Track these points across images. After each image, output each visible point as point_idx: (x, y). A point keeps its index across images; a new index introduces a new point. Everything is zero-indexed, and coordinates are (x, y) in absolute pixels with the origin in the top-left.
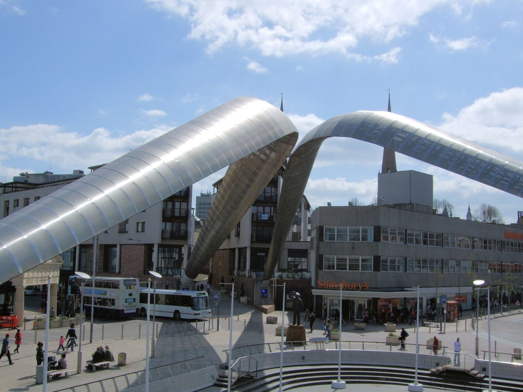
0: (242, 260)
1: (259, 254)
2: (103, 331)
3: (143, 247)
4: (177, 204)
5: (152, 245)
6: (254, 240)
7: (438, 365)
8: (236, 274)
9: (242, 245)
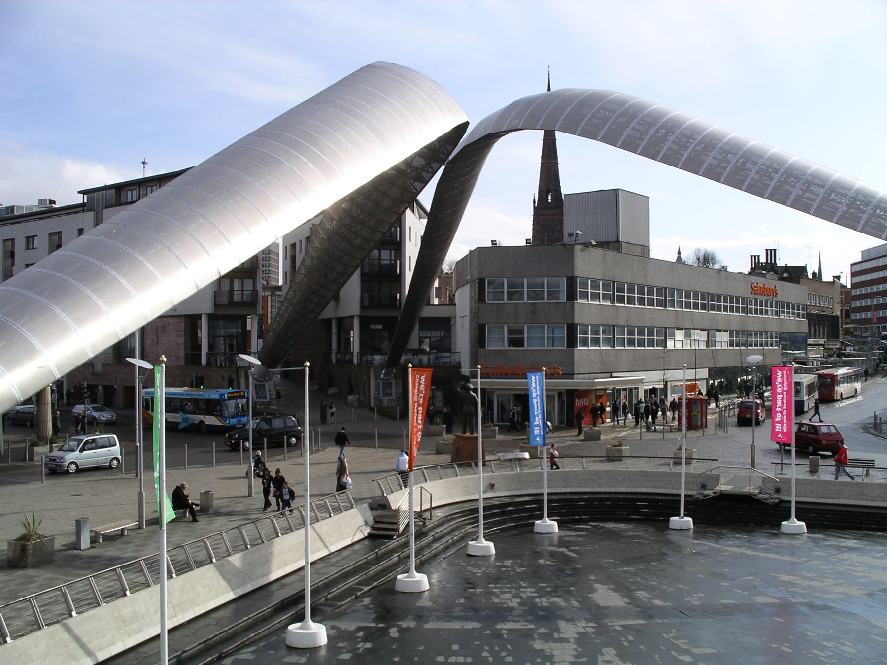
0: (343, 340)
1: (373, 327)
2: (323, 541)
3: (183, 320)
4: (237, 285)
5: (199, 317)
6: (366, 304)
7: (704, 487)
8: (334, 361)
9: (342, 313)
